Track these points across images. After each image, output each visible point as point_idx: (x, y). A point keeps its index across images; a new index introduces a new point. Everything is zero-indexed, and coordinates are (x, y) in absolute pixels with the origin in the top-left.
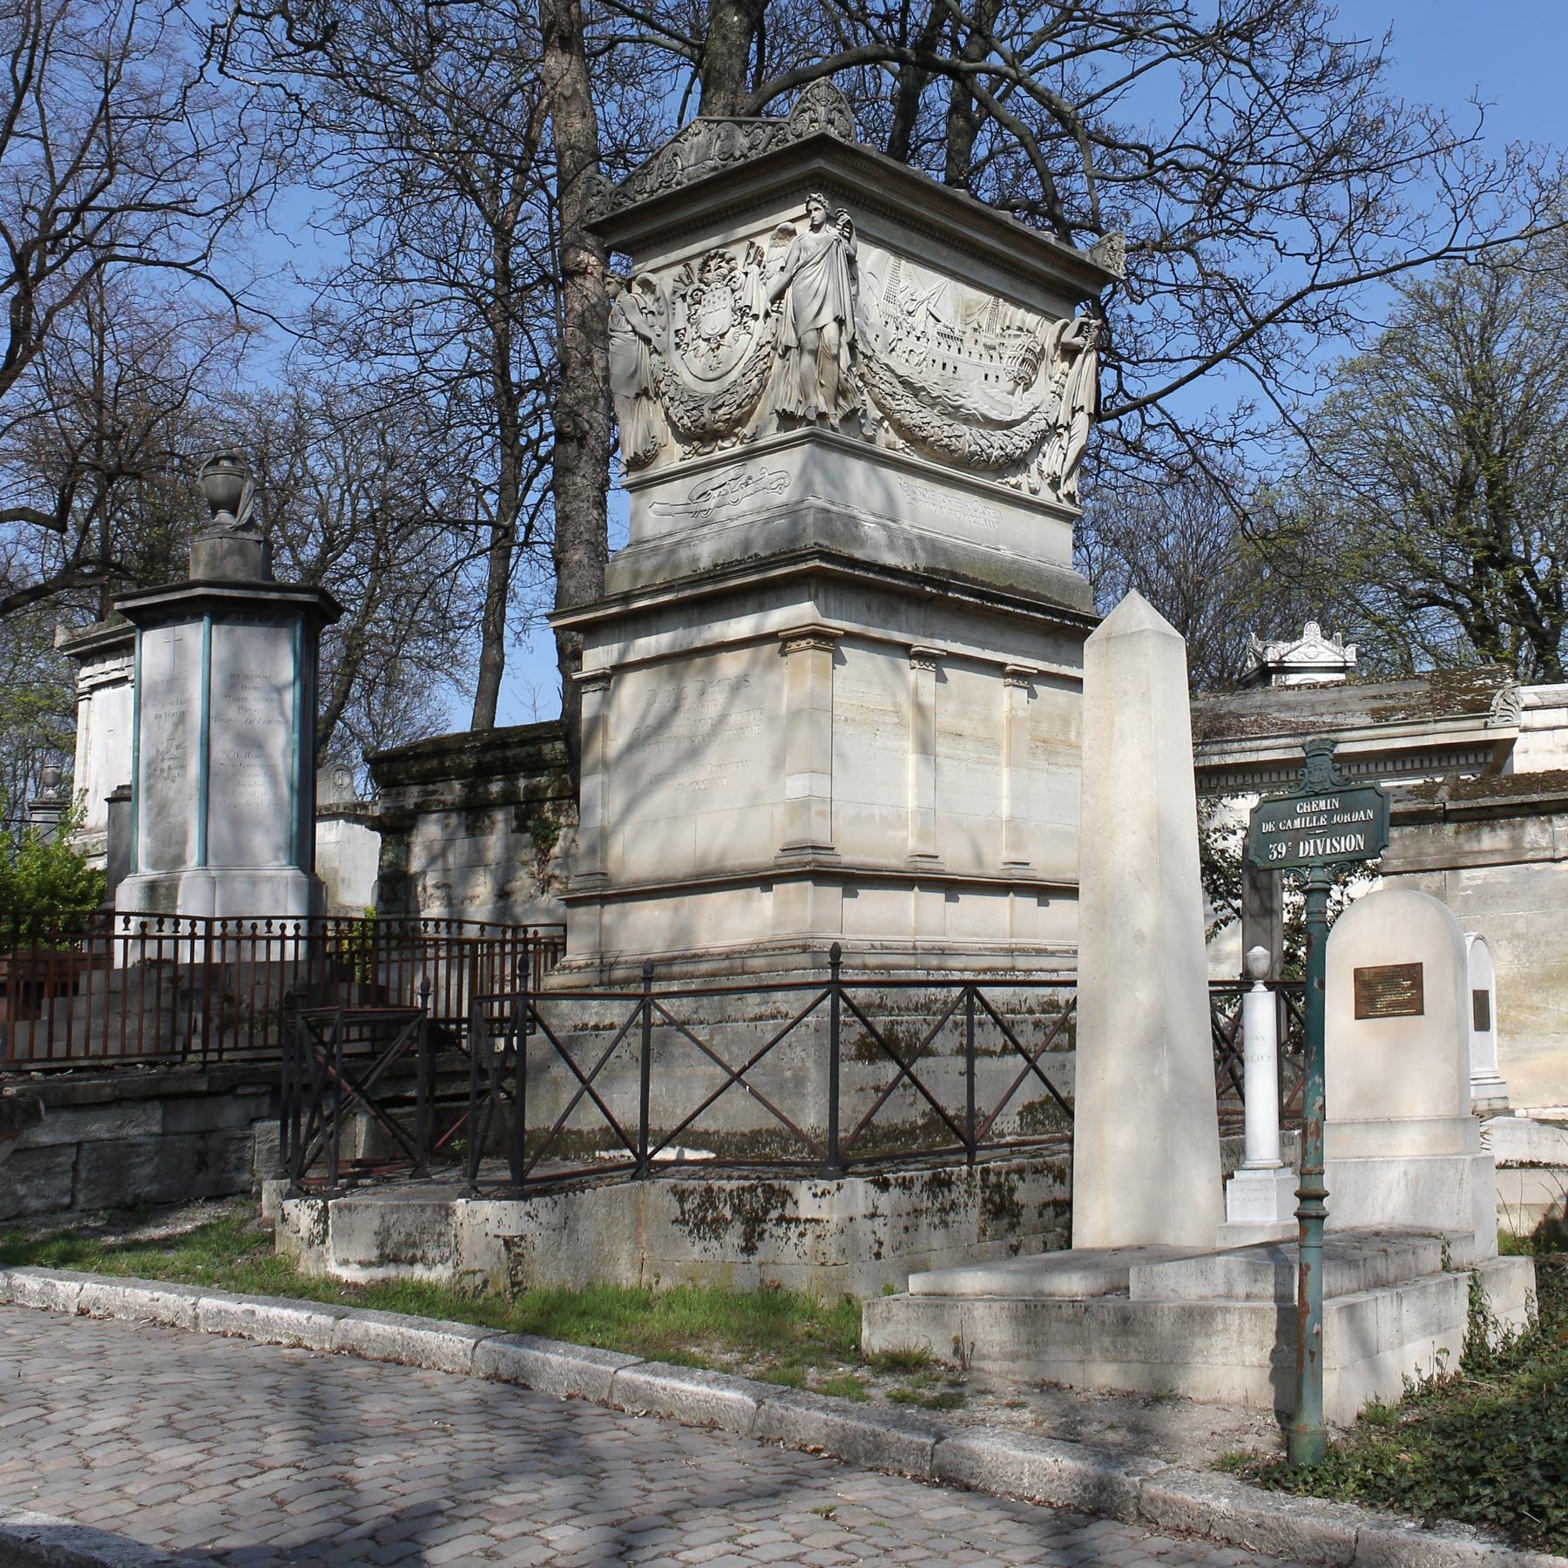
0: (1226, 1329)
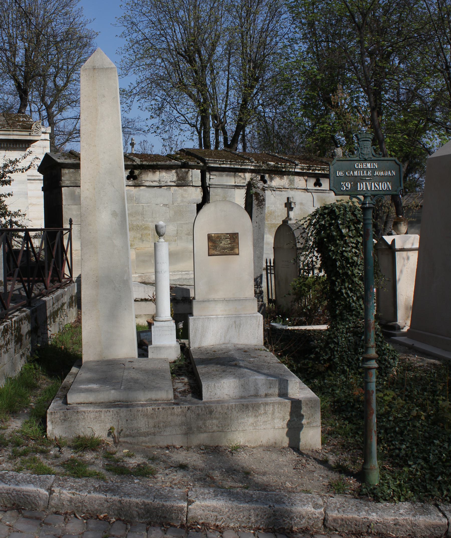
0: (265, 413)
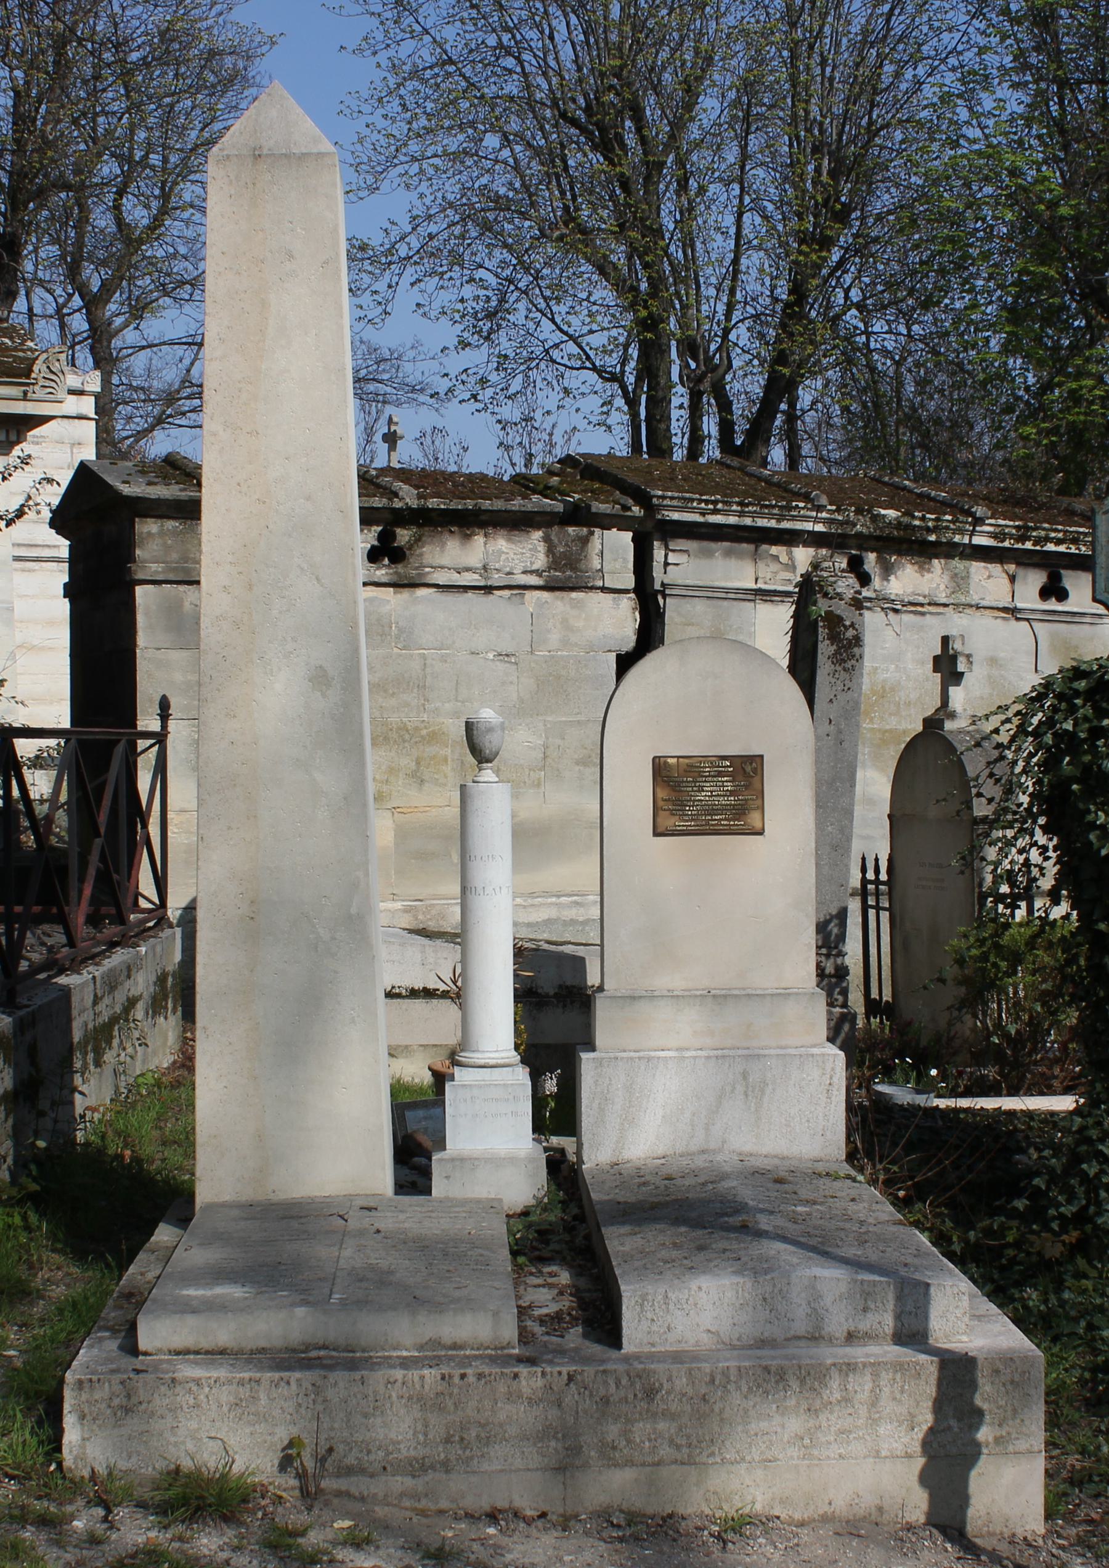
0: (846, 1400)
